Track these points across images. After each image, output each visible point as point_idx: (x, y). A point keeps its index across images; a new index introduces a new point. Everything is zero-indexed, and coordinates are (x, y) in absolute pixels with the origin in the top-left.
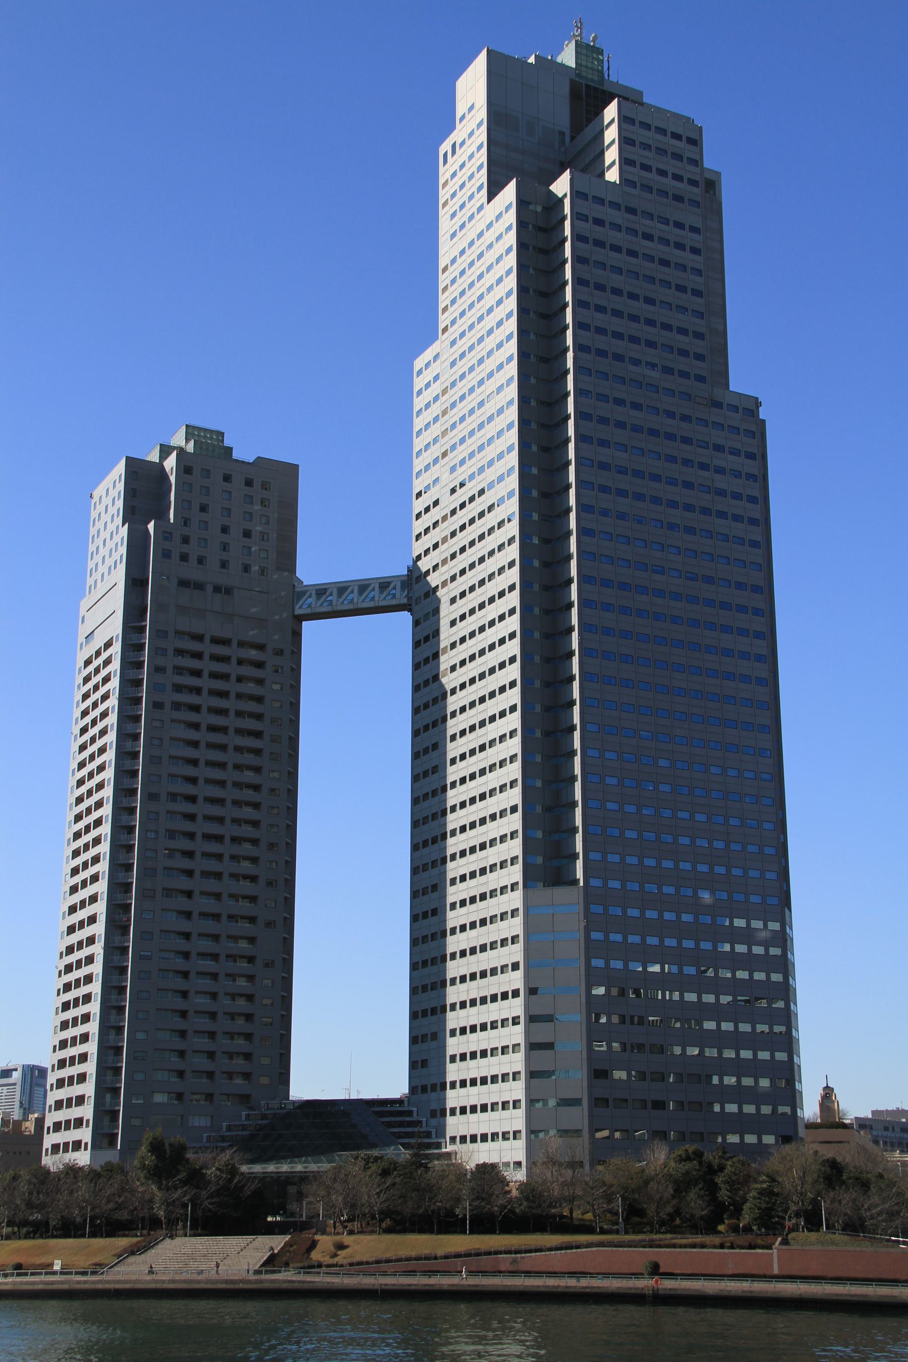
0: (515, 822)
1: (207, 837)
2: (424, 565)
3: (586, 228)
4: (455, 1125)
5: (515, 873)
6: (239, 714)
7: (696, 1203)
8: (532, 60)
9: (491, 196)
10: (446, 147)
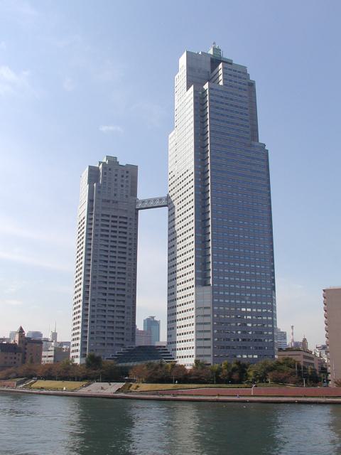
0: (193, 268)
1: (111, 272)
2: (170, 194)
3: (213, 98)
4: (179, 353)
5: (193, 283)
6: (120, 227)
7: (235, 376)
8: (200, 53)
9: (188, 89)
10: (176, 77)
